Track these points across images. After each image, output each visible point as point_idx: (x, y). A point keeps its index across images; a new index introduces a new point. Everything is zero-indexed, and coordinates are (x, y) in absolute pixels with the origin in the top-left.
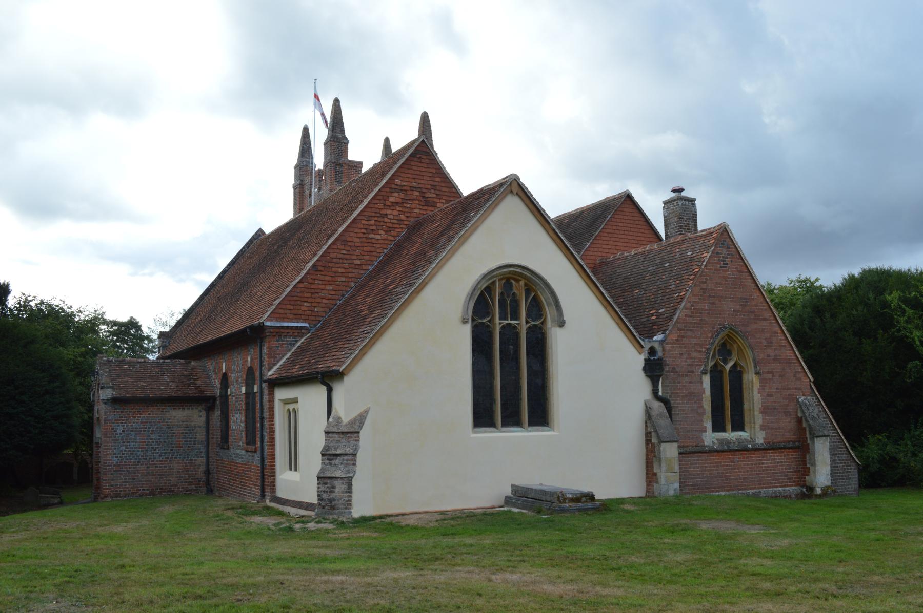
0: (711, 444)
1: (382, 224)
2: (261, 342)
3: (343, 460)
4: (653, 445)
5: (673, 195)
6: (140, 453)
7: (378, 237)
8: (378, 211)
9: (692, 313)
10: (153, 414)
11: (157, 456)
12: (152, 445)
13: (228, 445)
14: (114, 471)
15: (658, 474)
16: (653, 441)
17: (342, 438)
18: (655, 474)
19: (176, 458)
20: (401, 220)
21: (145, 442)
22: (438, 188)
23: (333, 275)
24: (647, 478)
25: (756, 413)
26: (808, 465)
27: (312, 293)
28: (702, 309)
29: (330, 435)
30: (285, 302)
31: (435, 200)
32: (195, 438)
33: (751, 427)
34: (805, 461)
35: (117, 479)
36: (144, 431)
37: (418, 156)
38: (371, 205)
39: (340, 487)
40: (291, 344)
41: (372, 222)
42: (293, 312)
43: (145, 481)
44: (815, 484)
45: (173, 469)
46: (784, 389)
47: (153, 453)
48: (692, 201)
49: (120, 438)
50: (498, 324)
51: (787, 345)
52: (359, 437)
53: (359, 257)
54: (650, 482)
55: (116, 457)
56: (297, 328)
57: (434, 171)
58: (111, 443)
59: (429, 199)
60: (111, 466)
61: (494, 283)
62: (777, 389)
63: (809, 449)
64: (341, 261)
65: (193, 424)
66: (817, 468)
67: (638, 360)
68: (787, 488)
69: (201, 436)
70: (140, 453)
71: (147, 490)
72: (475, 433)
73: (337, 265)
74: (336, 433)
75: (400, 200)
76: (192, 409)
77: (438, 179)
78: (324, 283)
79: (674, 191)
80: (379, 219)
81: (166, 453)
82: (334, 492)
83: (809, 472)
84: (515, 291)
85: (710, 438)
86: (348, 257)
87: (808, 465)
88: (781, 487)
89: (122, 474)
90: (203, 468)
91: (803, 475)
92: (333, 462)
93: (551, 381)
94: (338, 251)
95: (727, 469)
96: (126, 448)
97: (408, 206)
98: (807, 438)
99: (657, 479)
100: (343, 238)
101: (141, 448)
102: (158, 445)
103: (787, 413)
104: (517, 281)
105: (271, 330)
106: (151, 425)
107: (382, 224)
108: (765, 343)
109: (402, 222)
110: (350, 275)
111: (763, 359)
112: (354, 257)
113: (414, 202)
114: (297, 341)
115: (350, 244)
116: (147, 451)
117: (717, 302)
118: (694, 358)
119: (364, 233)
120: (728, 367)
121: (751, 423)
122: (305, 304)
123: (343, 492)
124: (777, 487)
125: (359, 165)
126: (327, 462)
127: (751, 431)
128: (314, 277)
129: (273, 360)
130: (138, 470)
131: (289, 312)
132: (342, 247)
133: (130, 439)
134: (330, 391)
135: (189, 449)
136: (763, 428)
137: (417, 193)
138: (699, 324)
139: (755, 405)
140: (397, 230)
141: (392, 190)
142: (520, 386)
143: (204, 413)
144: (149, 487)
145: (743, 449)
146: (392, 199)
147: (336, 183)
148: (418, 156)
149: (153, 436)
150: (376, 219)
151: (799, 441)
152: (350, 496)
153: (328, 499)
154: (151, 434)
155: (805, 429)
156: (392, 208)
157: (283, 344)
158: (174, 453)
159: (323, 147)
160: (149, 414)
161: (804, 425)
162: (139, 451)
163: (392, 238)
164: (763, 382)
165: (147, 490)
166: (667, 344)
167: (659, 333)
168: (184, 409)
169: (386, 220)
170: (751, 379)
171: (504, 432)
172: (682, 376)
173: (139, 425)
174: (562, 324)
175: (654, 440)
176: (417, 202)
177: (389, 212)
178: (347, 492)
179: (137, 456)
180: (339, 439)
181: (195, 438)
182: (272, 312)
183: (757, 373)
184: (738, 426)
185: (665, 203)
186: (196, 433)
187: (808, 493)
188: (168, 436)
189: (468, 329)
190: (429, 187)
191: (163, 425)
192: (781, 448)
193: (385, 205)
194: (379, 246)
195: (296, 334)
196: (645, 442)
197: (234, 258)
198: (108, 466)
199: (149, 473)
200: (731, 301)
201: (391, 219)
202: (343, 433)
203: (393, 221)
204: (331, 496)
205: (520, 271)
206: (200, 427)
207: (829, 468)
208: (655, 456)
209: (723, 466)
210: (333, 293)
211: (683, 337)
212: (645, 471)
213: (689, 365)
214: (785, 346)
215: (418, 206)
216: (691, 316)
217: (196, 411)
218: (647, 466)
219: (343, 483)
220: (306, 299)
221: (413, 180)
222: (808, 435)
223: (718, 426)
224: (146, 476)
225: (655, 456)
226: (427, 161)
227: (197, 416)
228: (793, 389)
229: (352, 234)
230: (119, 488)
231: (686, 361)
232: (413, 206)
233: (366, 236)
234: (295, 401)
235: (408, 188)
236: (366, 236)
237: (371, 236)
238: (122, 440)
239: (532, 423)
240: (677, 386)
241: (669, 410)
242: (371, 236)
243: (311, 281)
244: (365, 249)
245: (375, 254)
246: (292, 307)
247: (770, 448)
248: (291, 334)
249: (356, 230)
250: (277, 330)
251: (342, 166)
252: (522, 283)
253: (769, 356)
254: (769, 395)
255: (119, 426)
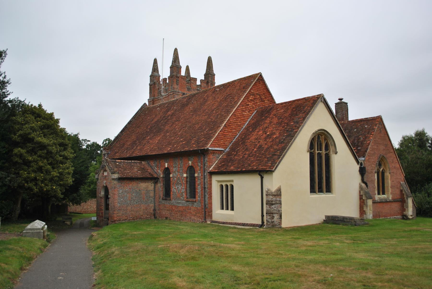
0: (377, 200)
1: (247, 108)
2: (204, 156)
3: (276, 206)
4: (364, 200)
5: (339, 101)
6: (129, 202)
7: (246, 114)
8: (245, 103)
9: (372, 149)
10: (133, 185)
11: (135, 203)
12: (133, 198)
13: (171, 199)
14: (118, 210)
15: (366, 211)
16: (363, 198)
17: (274, 197)
18: (365, 211)
19: (142, 204)
20: (254, 107)
21: (130, 197)
22: (265, 94)
23: (231, 129)
24: (360, 212)
25: (389, 188)
26: (405, 208)
27: (224, 136)
28: (375, 148)
29: (268, 196)
30: (215, 140)
31: (264, 99)
32: (150, 195)
33: (387, 193)
34: (404, 206)
35: (120, 213)
36: (130, 192)
37: (259, 81)
38: (244, 101)
39: (276, 217)
40: (217, 157)
41: (244, 108)
42: (218, 144)
43: (131, 214)
44: (407, 215)
45: (141, 209)
46: (397, 179)
47: (133, 202)
48: (346, 103)
49: (121, 195)
50: (317, 152)
51: (398, 162)
52: (281, 197)
53: (240, 122)
54: (362, 214)
55: (119, 203)
56: (220, 150)
57: (264, 87)
58: (117, 197)
59: (262, 99)
60: (117, 207)
61: (315, 136)
62: (395, 179)
63: (405, 201)
64: (234, 123)
65: (149, 189)
66: (409, 209)
67: (357, 167)
68: (398, 216)
69: (152, 194)
70: (129, 202)
71: (131, 218)
72: (311, 195)
73: (233, 125)
74: (271, 195)
75: (253, 99)
76: (149, 182)
77: (265, 91)
78: (228, 132)
79: (339, 99)
80: (246, 106)
81: (139, 202)
82: (274, 219)
83: (405, 210)
84: (321, 140)
85: (377, 197)
86: (236, 121)
87: (405, 208)
88: (396, 216)
89: (121, 211)
90: (153, 208)
91: (403, 211)
92: (271, 207)
93: (332, 175)
94: (233, 119)
95: (382, 209)
96: (123, 200)
97: (256, 101)
98: (404, 198)
99: (365, 213)
100: (235, 114)
101: (129, 199)
102: (136, 198)
103: (397, 188)
104: (322, 135)
105: (211, 151)
106: (133, 190)
107: (247, 108)
108: (392, 162)
109: (254, 108)
110: (237, 129)
111: (391, 167)
112: (238, 122)
113: (258, 100)
114: (219, 156)
115: (237, 116)
116: (131, 201)
117: (379, 146)
118: (373, 167)
119: (241, 112)
120: (381, 170)
121: (387, 191)
122: (222, 141)
123: (278, 219)
124: (395, 216)
125: (195, 79)
126: (269, 207)
127: (387, 194)
128: (225, 129)
129: (211, 164)
130: (128, 209)
131: (216, 144)
132: (234, 117)
133: (125, 196)
134: (262, 178)
135: (147, 200)
136: (391, 193)
137: (258, 96)
138: (374, 154)
139: (389, 185)
140: (252, 111)
141: (251, 95)
142: (322, 177)
143: (153, 185)
144: (132, 216)
145: (386, 202)
146: (250, 98)
147: (176, 85)
148: (259, 81)
149: (133, 194)
150: (245, 106)
151: (401, 199)
152: (281, 220)
153: (272, 222)
154: (133, 193)
155: (404, 194)
156: (251, 102)
157: (215, 157)
158: (142, 201)
159: (170, 69)
160: (132, 185)
161: (403, 192)
162: (128, 201)
163: (251, 115)
164: (391, 176)
165: (131, 218)
166: (365, 161)
167: (361, 157)
168: (146, 182)
169: (248, 107)
170: (387, 175)
171: (319, 195)
172: (369, 173)
173: (128, 190)
174: (336, 153)
175: (364, 198)
176: (259, 100)
177: (249, 103)
178: (280, 219)
179: (128, 203)
180: (272, 197)
181: (150, 195)
182: (211, 144)
183: (390, 173)
184: (384, 193)
185: (336, 104)
186: (150, 193)
187: (405, 217)
188: (139, 194)
189: (309, 153)
190: (262, 94)
191: (138, 189)
192: (396, 201)
193: (248, 100)
194: (246, 117)
195: (219, 153)
196: (359, 199)
197: (135, 115)
198: (116, 207)
199: (132, 210)
200: (383, 145)
201: (250, 106)
202: (274, 195)
203: (251, 107)
204: (273, 221)
205: (324, 132)
206: (152, 190)
207: (412, 209)
208: (364, 204)
209: (381, 208)
210: (231, 136)
211: (370, 159)
212: (359, 210)
213: (371, 169)
214: (397, 163)
215: (259, 102)
216: (371, 151)
217: (150, 183)
218: (360, 208)
219: (278, 215)
220: (222, 139)
221: (257, 91)
222: (405, 196)
223: (379, 194)
224: (131, 212)
225: (364, 204)
226: (262, 83)
227: (150, 186)
228: (399, 179)
229: (237, 112)
230: (120, 217)
231: (370, 168)
232: (257, 101)
233: (242, 113)
234: (232, 181)
235: (255, 94)
236: (242, 113)
237: (244, 113)
238: (121, 196)
239: (327, 192)
240: (368, 177)
241: (367, 186)
242: (244, 113)
243: (224, 131)
244: (242, 118)
245: (245, 121)
246: (217, 142)
247: (394, 201)
248: (218, 153)
249: (239, 111)
250: (213, 151)
251: (179, 78)
252: (323, 137)
253: (393, 166)
254: (393, 181)
255: (120, 190)
